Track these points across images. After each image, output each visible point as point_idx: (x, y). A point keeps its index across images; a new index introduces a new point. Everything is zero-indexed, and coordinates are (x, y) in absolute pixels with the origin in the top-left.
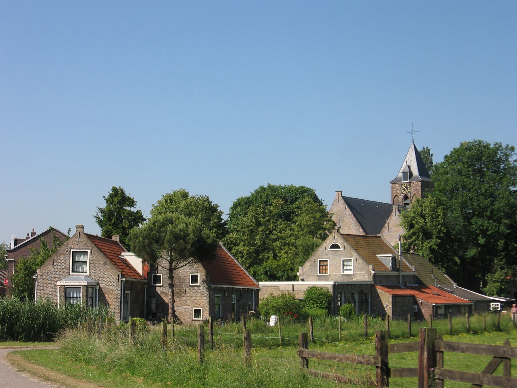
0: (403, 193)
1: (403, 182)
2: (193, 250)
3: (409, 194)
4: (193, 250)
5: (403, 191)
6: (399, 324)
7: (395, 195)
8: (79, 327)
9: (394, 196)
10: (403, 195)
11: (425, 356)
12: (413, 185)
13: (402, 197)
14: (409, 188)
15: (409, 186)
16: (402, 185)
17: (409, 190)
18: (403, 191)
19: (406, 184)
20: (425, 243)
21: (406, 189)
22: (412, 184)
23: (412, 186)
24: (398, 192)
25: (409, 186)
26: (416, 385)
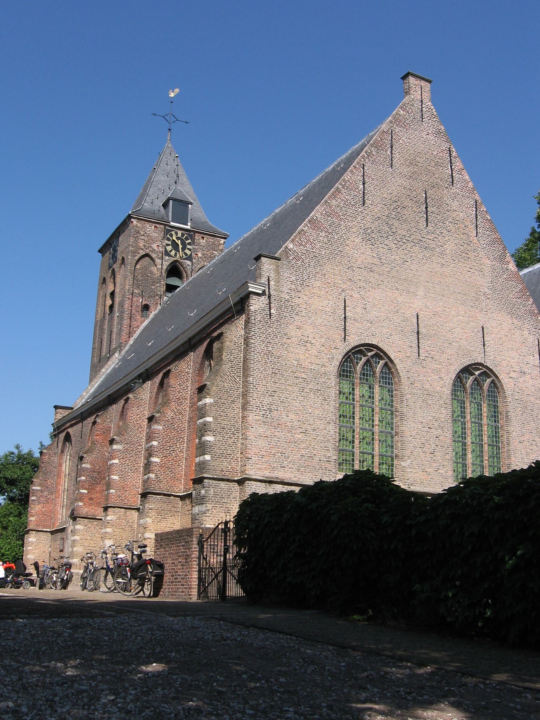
0: (170, 256)
1: (172, 224)
2: (521, 495)
3: (189, 262)
4: (521, 495)
5: (169, 248)
6: (502, 379)
7: (142, 253)
8: (18, 508)
9: (139, 256)
10: (167, 262)
11: (102, 379)
12: (203, 242)
13: (166, 264)
14: (188, 247)
15: (189, 241)
16: (167, 232)
17: (188, 252)
18: (169, 248)
19: (180, 233)
20: (86, 641)
21: (181, 246)
22: (197, 237)
23: (199, 245)
24: (154, 246)
25: (189, 241)
26: (148, 590)
